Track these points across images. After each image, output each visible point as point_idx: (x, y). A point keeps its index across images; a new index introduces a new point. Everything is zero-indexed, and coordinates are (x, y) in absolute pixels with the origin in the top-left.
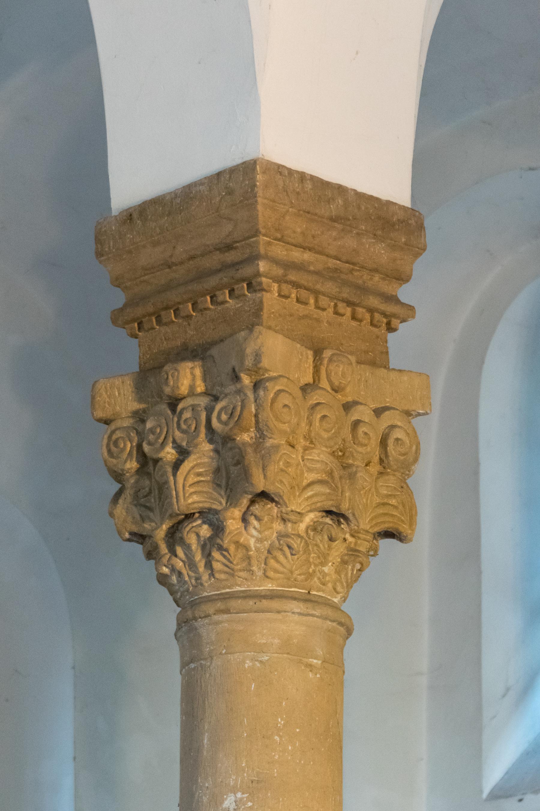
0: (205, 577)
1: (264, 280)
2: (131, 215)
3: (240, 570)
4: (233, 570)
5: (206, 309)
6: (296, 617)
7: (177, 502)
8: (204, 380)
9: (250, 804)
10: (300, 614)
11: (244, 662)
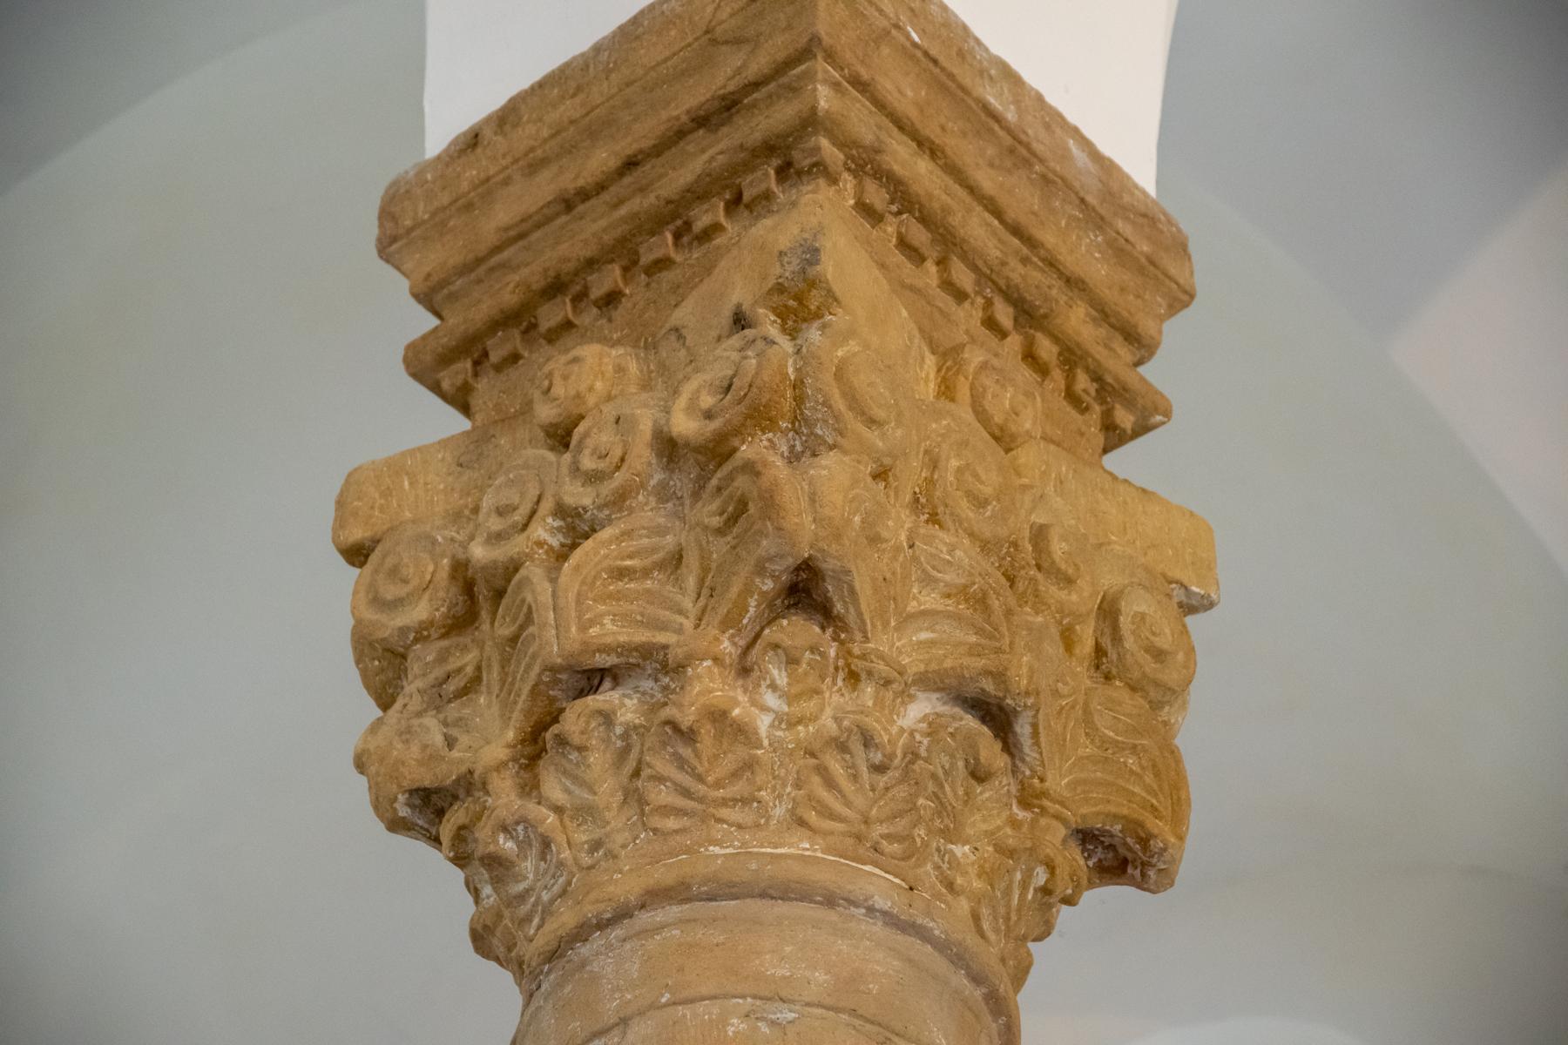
11: (723, 1021)
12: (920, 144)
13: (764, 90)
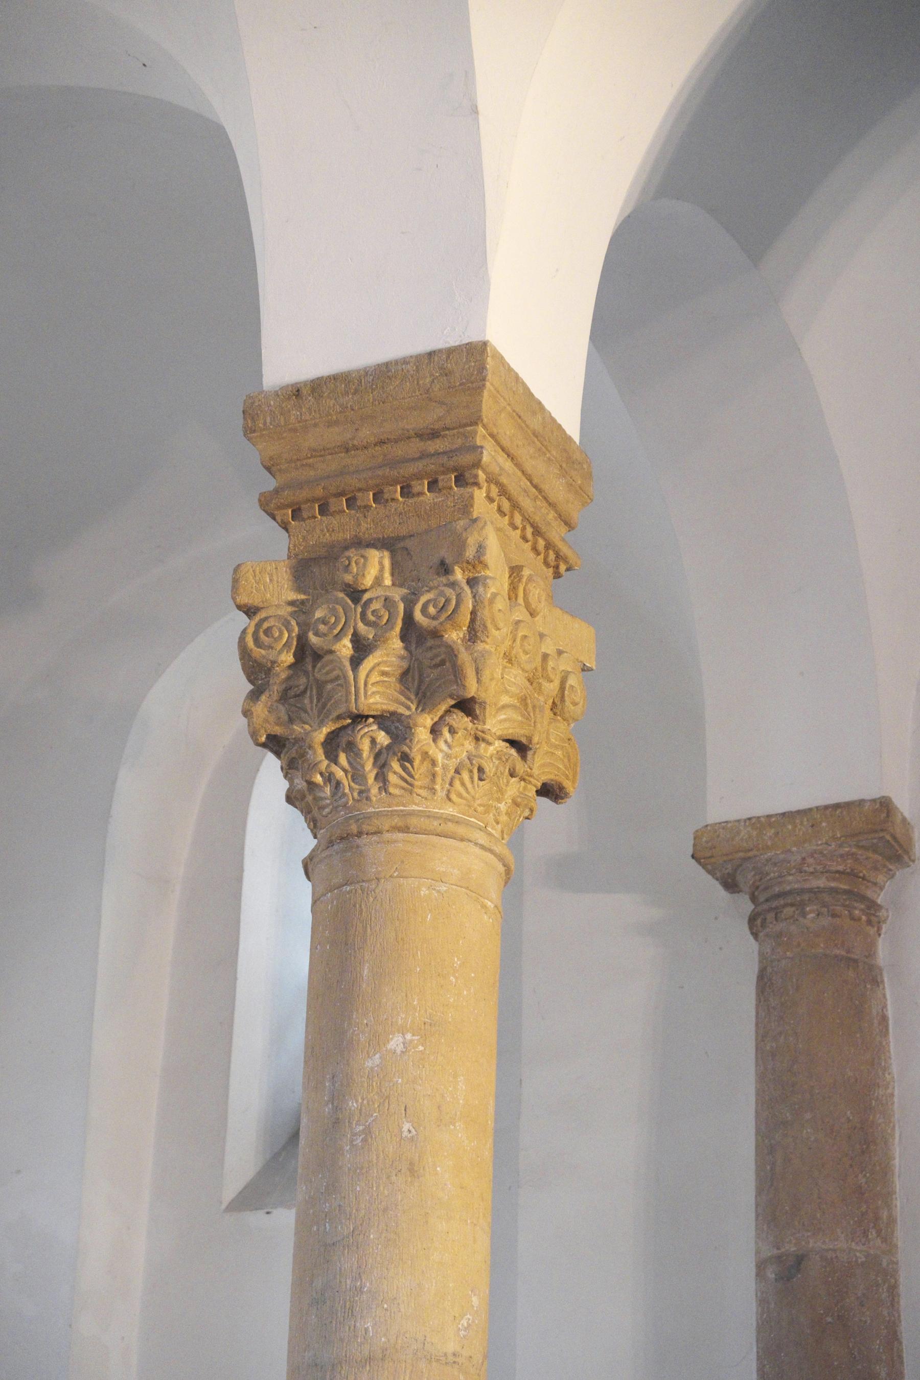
0: (374, 791)
1: (480, 473)
2: (298, 391)
3: (421, 788)
4: (411, 785)
5: (393, 499)
6: (477, 850)
7: (356, 700)
8: (392, 575)
9: (421, 1048)
10: (482, 847)
12: (508, 456)
13: (452, 432)
